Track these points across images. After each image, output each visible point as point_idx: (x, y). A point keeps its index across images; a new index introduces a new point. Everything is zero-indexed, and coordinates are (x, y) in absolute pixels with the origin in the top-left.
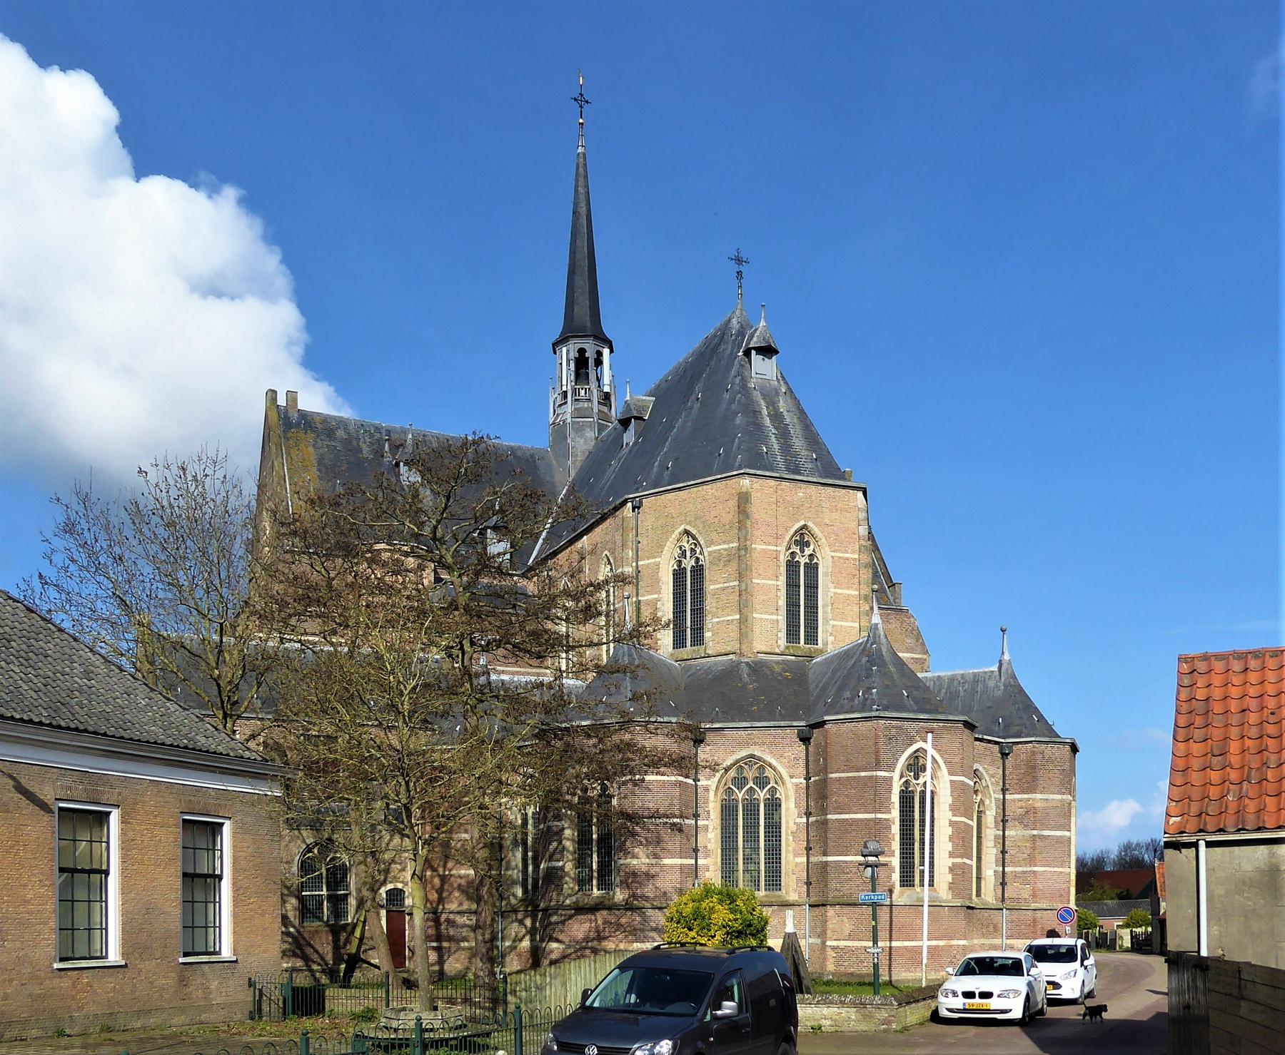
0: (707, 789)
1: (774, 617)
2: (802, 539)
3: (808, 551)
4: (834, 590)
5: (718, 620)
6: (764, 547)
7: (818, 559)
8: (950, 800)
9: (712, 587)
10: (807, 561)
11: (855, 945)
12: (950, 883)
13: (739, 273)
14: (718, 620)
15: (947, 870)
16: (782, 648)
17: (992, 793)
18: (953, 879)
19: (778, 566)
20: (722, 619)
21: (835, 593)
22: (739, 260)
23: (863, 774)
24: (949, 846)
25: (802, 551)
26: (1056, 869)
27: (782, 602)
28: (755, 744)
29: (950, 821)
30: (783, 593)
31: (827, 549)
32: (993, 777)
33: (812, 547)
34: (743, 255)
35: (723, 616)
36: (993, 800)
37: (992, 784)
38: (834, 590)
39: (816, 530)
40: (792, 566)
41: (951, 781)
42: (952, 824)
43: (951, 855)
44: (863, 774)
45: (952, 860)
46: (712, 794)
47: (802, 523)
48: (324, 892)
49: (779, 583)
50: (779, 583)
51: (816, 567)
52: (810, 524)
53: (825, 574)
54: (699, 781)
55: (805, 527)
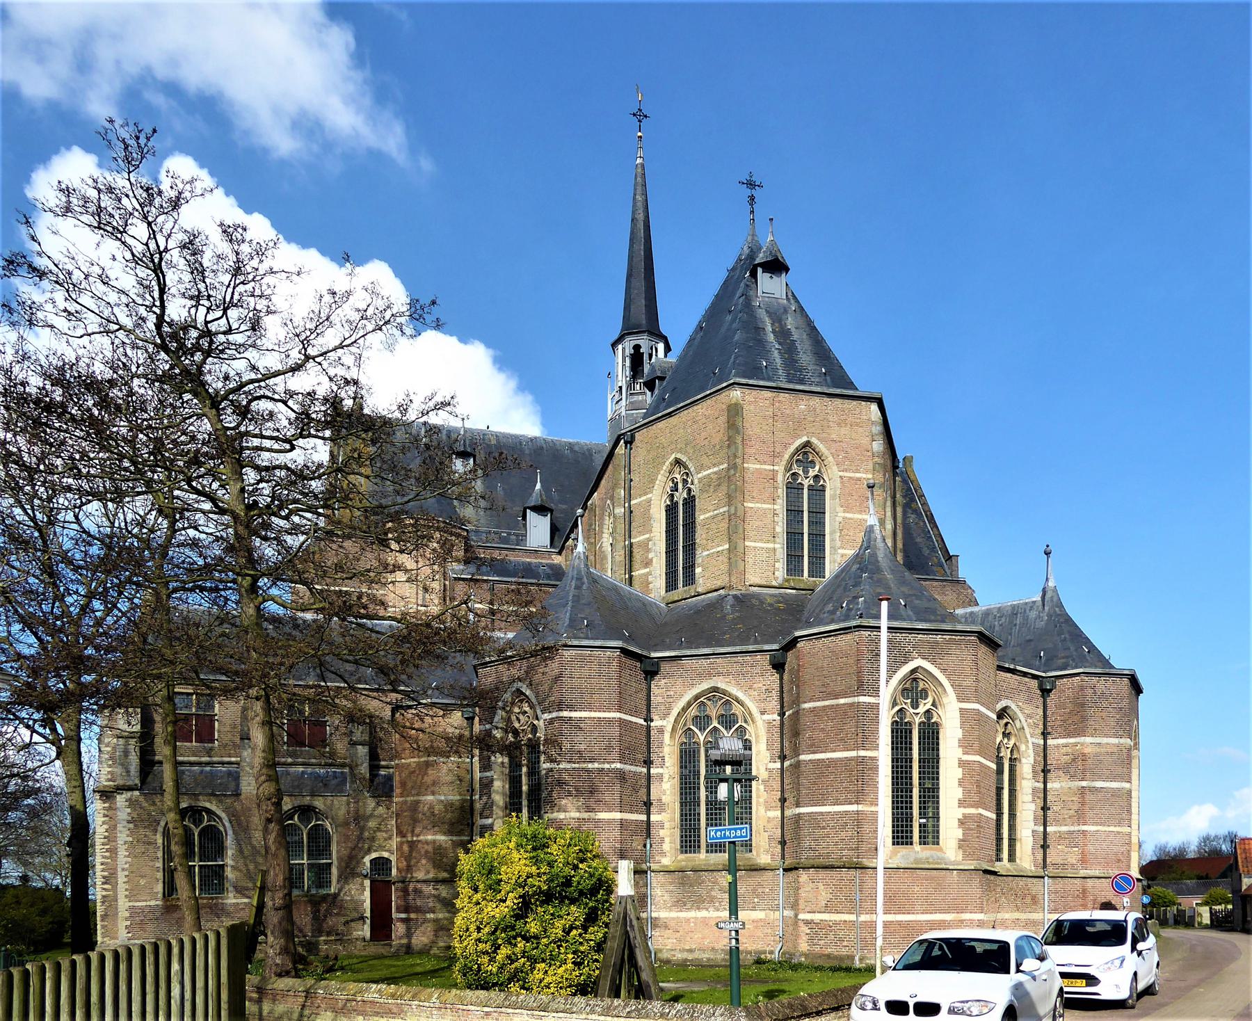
1: (771, 545)
2: (805, 455)
4: (843, 515)
6: (758, 466)
7: (824, 481)
8: (959, 733)
9: (702, 517)
13: (752, 198)
15: (956, 823)
16: (780, 580)
17: (1028, 736)
24: (959, 793)
25: (806, 472)
27: (781, 528)
28: (719, 674)
31: (835, 468)
36: (1030, 745)
37: (1029, 725)
38: (843, 515)
39: (821, 447)
40: (793, 488)
42: (962, 763)
43: (962, 803)
44: (842, 701)
46: (667, 736)
47: (805, 439)
49: (776, 507)
50: (776, 507)
51: (823, 489)
52: (814, 440)
53: (833, 497)
54: (652, 720)
55: (807, 444)
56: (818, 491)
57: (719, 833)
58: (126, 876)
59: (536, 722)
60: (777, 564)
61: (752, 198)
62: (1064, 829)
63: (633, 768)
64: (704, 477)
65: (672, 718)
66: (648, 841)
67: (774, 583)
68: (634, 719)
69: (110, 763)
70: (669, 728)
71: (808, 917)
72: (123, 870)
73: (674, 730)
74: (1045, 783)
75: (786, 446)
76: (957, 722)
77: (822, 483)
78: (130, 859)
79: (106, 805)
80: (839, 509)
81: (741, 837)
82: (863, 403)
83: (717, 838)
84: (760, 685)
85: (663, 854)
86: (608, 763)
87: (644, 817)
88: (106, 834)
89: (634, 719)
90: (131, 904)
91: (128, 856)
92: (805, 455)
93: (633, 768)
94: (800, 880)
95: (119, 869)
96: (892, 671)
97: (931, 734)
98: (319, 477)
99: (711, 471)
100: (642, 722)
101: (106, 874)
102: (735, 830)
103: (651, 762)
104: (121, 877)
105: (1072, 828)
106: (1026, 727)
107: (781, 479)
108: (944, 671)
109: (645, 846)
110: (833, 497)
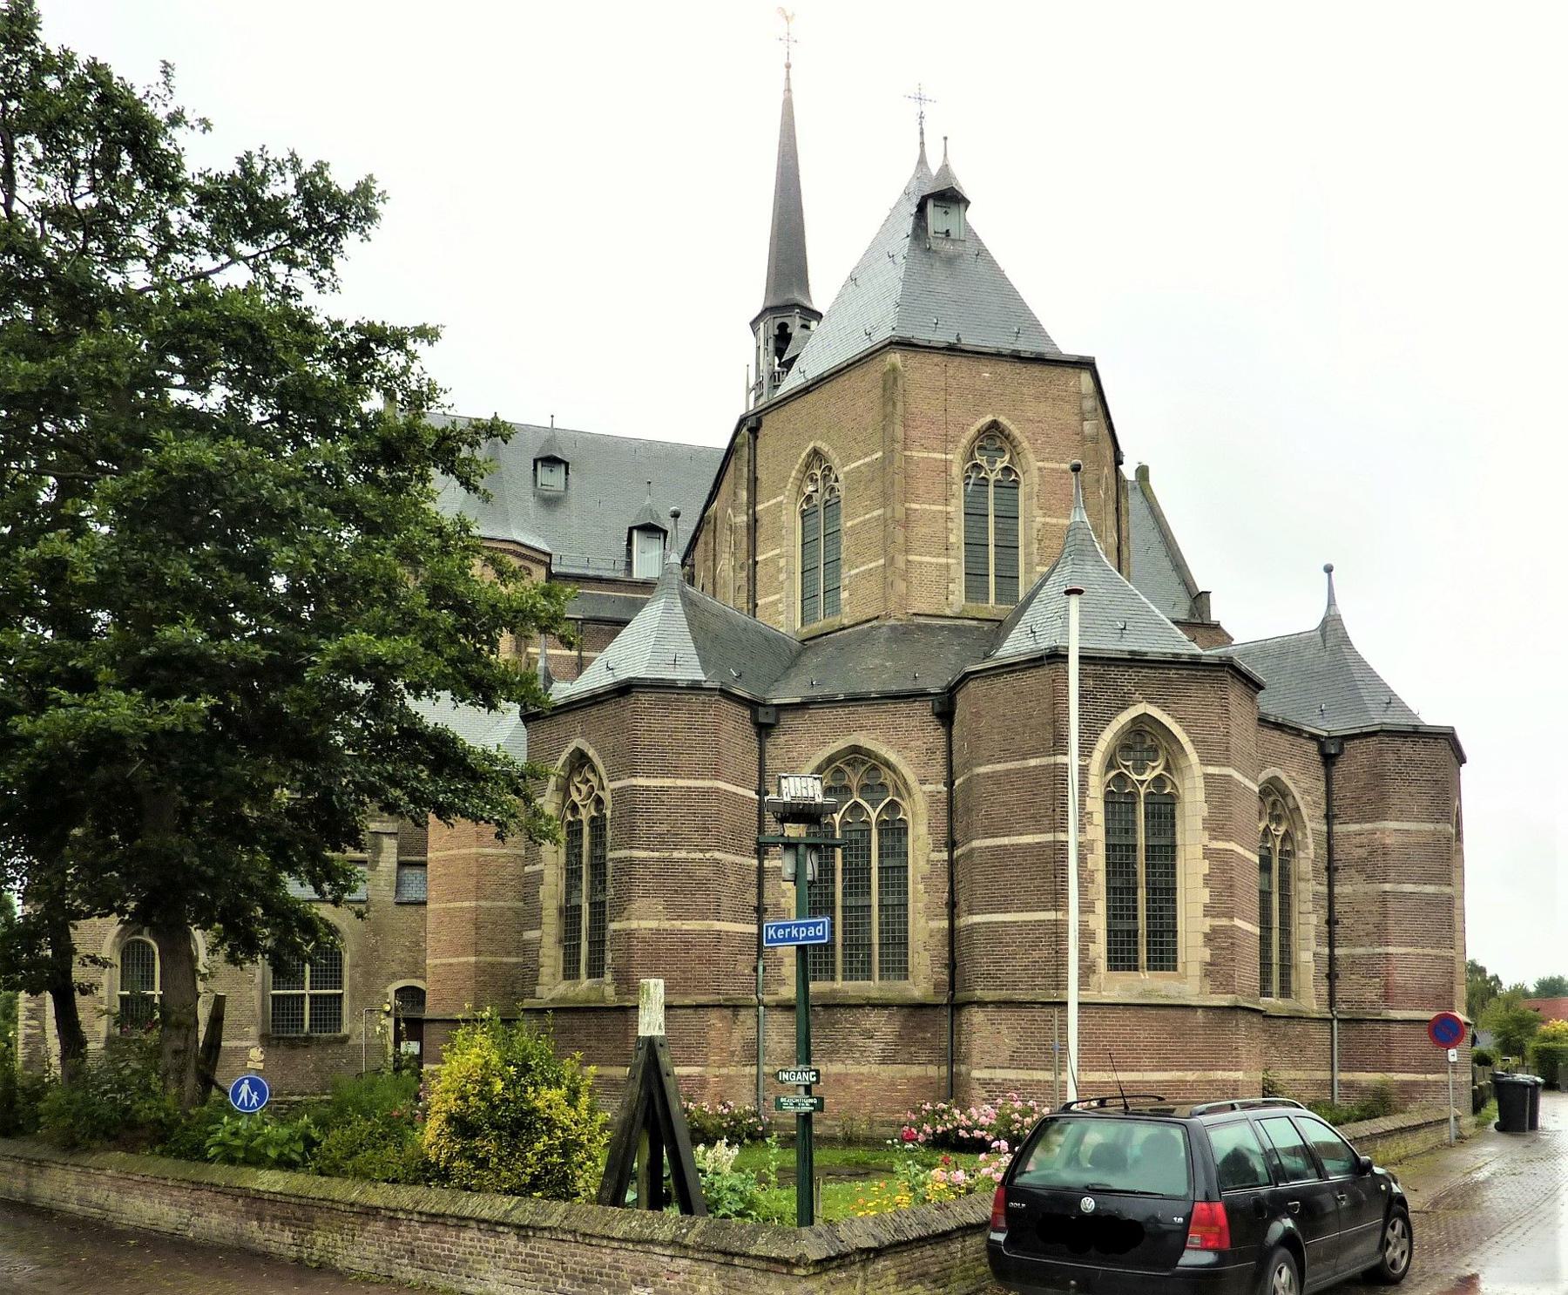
1: (943, 560)
4: (1043, 520)
5: (857, 571)
7: (1017, 475)
8: (1204, 810)
9: (849, 524)
11: (1021, 1077)
14: (857, 571)
15: (1200, 939)
17: (1306, 818)
18: (1212, 955)
19: (949, 484)
20: (862, 569)
23: (1033, 762)
24: (1205, 896)
27: (957, 537)
28: (861, 728)
31: (1031, 457)
35: (863, 563)
37: (1307, 805)
38: (1043, 520)
41: (1206, 776)
42: (1208, 854)
43: (1209, 911)
44: (1033, 762)
45: (1209, 922)
47: (989, 418)
50: (949, 509)
52: (1002, 419)
54: (767, 793)
59: (601, 794)
62: (1360, 951)
64: (852, 471)
67: (948, 612)
68: (740, 791)
71: (984, 1074)
74: (1331, 885)
76: (1200, 795)
81: (816, 937)
86: (701, 851)
89: (740, 791)
93: (738, 859)
99: (861, 462)
100: (753, 795)
107: (956, 471)
108: (1179, 720)
109: (756, 969)
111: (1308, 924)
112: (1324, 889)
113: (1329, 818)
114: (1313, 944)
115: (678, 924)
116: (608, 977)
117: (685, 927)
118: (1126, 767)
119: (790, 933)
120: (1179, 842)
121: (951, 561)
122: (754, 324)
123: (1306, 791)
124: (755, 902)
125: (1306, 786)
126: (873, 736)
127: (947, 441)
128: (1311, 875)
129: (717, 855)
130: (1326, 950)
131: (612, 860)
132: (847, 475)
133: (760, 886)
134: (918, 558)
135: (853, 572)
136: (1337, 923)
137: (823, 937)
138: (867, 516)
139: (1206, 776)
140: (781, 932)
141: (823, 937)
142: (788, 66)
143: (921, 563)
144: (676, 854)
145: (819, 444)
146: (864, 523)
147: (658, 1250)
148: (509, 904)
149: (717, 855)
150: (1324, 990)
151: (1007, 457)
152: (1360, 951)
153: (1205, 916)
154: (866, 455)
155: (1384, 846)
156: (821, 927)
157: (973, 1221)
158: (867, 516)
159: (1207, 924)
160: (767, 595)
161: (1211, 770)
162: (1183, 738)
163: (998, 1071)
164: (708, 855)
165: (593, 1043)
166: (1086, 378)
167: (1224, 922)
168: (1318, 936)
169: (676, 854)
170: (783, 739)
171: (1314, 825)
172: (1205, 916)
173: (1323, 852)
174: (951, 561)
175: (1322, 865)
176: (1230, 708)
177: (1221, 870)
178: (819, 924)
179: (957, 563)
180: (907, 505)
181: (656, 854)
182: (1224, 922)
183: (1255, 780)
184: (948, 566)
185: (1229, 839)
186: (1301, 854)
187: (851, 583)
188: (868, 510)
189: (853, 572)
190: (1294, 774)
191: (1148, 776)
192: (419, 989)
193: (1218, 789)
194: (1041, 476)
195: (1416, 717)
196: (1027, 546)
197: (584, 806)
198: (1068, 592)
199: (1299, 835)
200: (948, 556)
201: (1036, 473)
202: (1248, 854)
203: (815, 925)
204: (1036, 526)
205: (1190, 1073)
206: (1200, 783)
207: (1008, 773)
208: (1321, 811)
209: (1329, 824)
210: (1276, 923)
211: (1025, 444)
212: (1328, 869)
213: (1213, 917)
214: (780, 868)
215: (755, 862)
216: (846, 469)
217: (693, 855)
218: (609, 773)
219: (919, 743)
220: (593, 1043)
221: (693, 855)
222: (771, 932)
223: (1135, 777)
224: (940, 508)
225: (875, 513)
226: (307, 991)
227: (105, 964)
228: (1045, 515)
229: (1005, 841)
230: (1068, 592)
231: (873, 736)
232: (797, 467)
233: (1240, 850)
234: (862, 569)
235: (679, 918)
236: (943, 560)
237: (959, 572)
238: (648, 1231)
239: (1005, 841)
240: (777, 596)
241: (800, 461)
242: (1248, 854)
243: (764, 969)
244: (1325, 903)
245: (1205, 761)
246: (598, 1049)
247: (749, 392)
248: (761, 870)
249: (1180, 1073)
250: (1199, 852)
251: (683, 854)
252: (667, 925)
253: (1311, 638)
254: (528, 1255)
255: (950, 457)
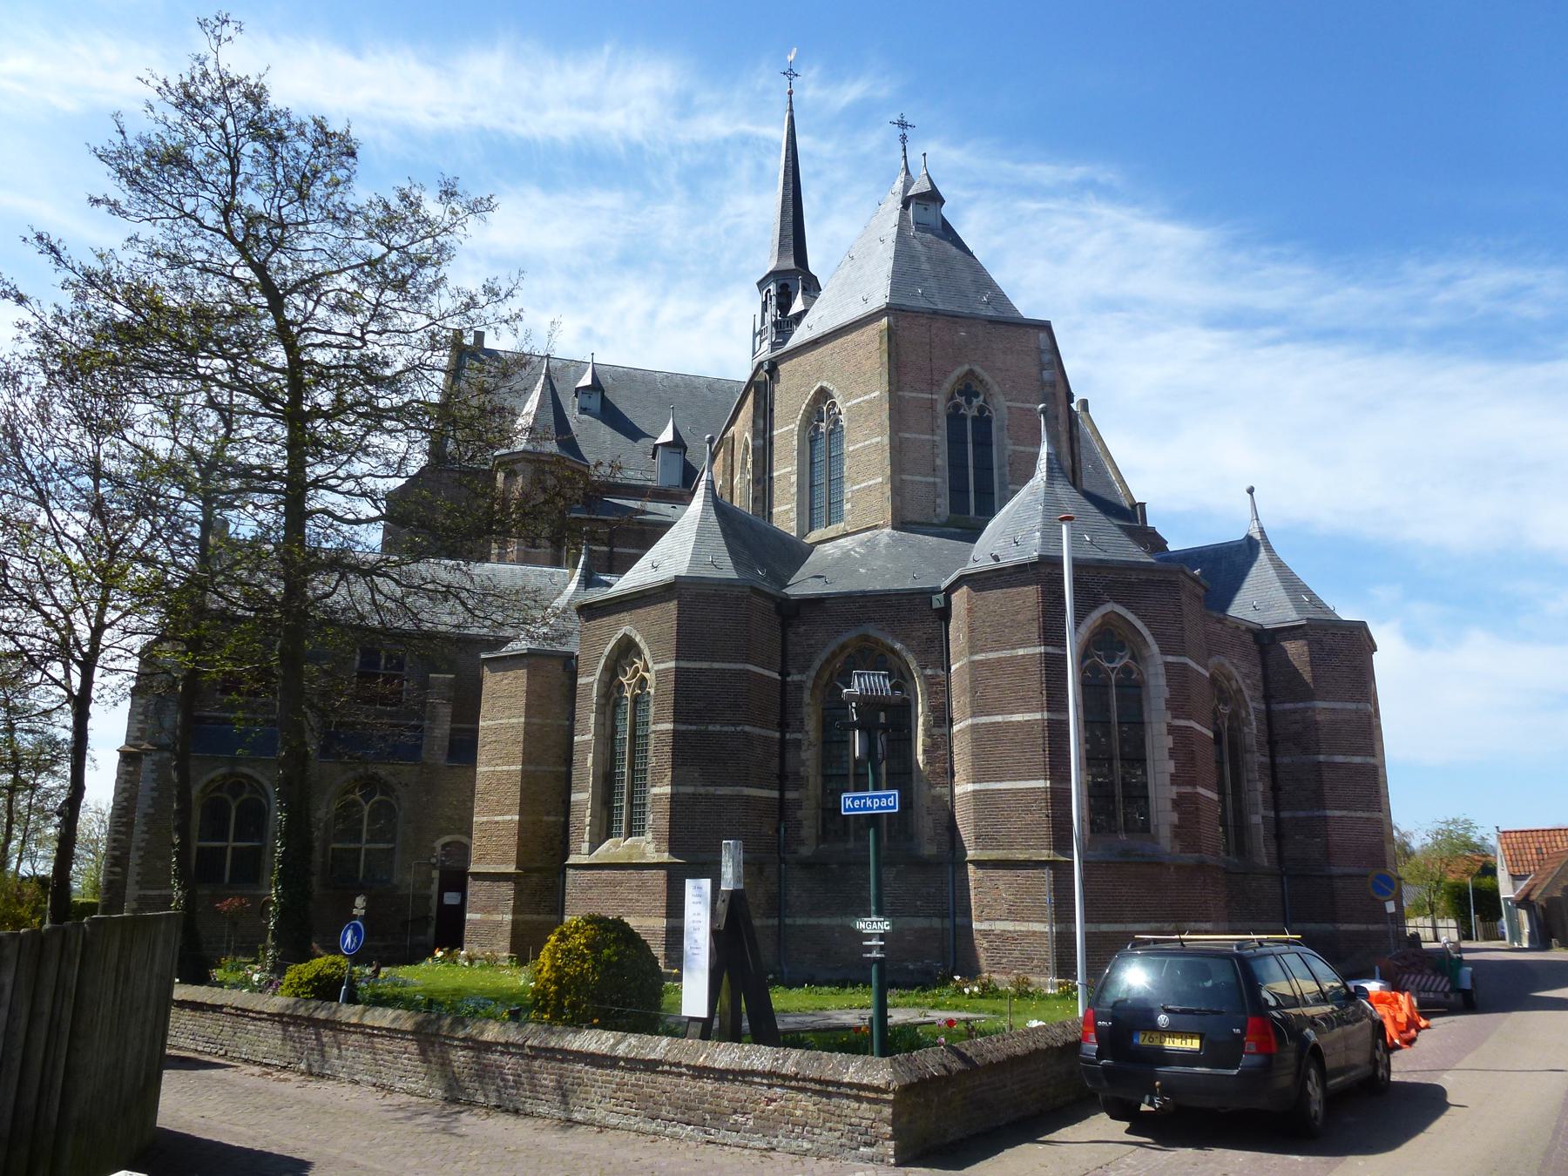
0: (800, 686)
1: (932, 479)
2: (969, 388)
3: (977, 402)
4: (1013, 447)
5: (858, 487)
6: (914, 395)
7: (990, 412)
8: (1166, 693)
9: (851, 449)
10: (976, 414)
11: (1018, 928)
12: (1176, 826)
13: (904, 138)
14: (858, 487)
15: (1169, 806)
16: (943, 519)
17: (1248, 700)
18: (1179, 818)
19: (934, 418)
20: (863, 485)
21: (1014, 451)
22: (903, 125)
23: (1021, 652)
24: (1171, 766)
25: (969, 402)
26: (1359, 814)
27: (942, 461)
28: (870, 620)
29: (1169, 725)
30: (943, 448)
31: (1002, 398)
32: (1249, 678)
33: (981, 398)
34: (908, 119)
35: (863, 481)
36: (1251, 711)
37: (1248, 686)
38: (1013, 447)
39: (986, 377)
40: (955, 418)
41: (1167, 664)
42: (1172, 730)
43: (1175, 780)
44: (1021, 652)
45: (1175, 789)
46: (807, 697)
47: (966, 367)
48: (364, 846)
49: (936, 438)
50: (936, 438)
51: (989, 420)
52: (977, 369)
53: (1001, 429)
54: (789, 675)
55: (971, 372)
56: (983, 423)
57: (856, 803)
58: (141, 857)
59: (646, 675)
60: (938, 501)
61: (904, 138)
62: (1301, 814)
63: (764, 732)
64: (853, 406)
65: (813, 673)
66: (783, 825)
67: (935, 521)
68: (766, 673)
69: (142, 717)
70: (810, 684)
71: (985, 926)
72: (138, 849)
73: (815, 685)
74: (1272, 757)
75: (946, 374)
76: (1163, 681)
77: (987, 413)
78: (147, 836)
79: (131, 769)
80: (1008, 441)
81: (888, 807)
82: (1031, 331)
83: (855, 809)
84: (919, 634)
85: (801, 842)
86: (733, 725)
87: (775, 794)
88: (125, 804)
89: (766, 673)
90: (142, 892)
91: (146, 832)
92: (969, 388)
93: (764, 732)
94: (389, 375)
95: (133, 849)
96: (1079, 618)
97: (1133, 689)
98: (182, 205)
99: (862, 399)
100: (776, 676)
101: (117, 853)
102: (879, 797)
103: (788, 725)
104: (134, 859)
105: (1310, 814)
106: (1243, 687)
107: (941, 408)
108: (1141, 617)
109: (778, 830)
110: (1001, 429)
111: (1258, 789)
112: (1266, 760)
113: (1268, 698)
114: (1262, 811)
115: (711, 789)
116: (649, 836)
117: (718, 793)
118: (1099, 657)
119: (865, 803)
120: (1146, 719)
121: (938, 480)
122: (762, 284)
123: (1246, 676)
124: (777, 771)
125: (1246, 671)
126: (880, 627)
127: (933, 385)
128: (1255, 748)
129: (747, 728)
130: (1272, 814)
131: (655, 732)
132: (849, 410)
133: (782, 757)
134: (909, 477)
135: (855, 488)
136: (1280, 789)
137: (894, 807)
138: (866, 443)
139: (1167, 664)
140: (857, 802)
141: (894, 807)
142: (790, 93)
143: (912, 482)
144: (711, 728)
145: (825, 384)
146: (865, 448)
147: (757, 1080)
148: (551, 769)
149: (747, 728)
150: (1273, 849)
151: (981, 398)
152: (1301, 814)
153: (1172, 784)
154: (866, 394)
155: (1316, 722)
156: (892, 799)
157: (1019, 1051)
158: (866, 443)
159: (1173, 791)
160: (780, 505)
161: (1170, 659)
162: (1145, 632)
163: (998, 923)
164: (739, 729)
165: (635, 896)
166: (1043, 335)
167: (1188, 789)
168: (1264, 801)
169: (711, 728)
170: (802, 629)
171: (1255, 704)
172: (1172, 784)
173: (1264, 727)
174: (938, 480)
175: (1264, 739)
176: (1183, 607)
177: (1183, 743)
178: (890, 796)
179: (942, 481)
180: (901, 434)
181: (694, 728)
182: (1188, 789)
183: (1206, 667)
184: (935, 484)
185: (1189, 718)
186: (1246, 730)
187: (852, 497)
188: (868, 437)
189: (855, 488)
190: (1235, 661)
191: (1118, 664)
192: (462, 843)
193: (1177, 675)
194: (1010, 413)
195: (1332, 612)
196: (1000, 468)
197: (629, 685)
198: (1062, 520)
199: (1244, 714)
200: (935, 476)
201: (1006, 410)
202: (1205, 731)
203: (887, 797)
204: (1007, 453)
205: (1166, 925)
206: (1161, 670)
207: (999, 660)
208: (1259, 694)
209: (1268, 705)
210: (1229, 791)
211: (996, 388)
212: (1269, 742)
213: (1179, 785)
214: (800, 740)
215: (777, 735)
216: (848, 404)
217: (725, 729)
218: (653, 656)
219: (919, 634)
220: (635, 896)
221: (725, 729)
222: (848, 802)
223: (1106, 665)
224: (927, 437)
225: (874, 440)
226: (231, 844)
227: (980, 864)
228: (1014, 444)
229: (999, 718)
230: (1062, 520)
231: (880, 627)
232: (807, 401)
233: (1198, 727)
234: (863, 485)
235: (714, 784)
236: (932, 479)
237: (944, 488)
238: (747, 1062)
239: (999, 718)
240: (789, 506)
241: (809, 397)
242: (1205, 731)
243: (786, 830)
244: (1269, 772)
245: (1164, 652)
246: (638, 901)
247: (755, 335)
248: (783, 741)
249: (1159, 925)
250: (1164, 729)
251: (718, 728)
252: (702, 790)
253: (1240, 546)
254: (633, 1085)
255: (935, 397)
